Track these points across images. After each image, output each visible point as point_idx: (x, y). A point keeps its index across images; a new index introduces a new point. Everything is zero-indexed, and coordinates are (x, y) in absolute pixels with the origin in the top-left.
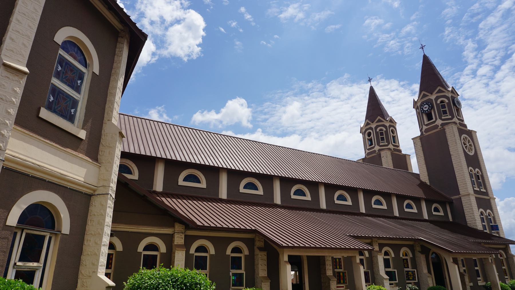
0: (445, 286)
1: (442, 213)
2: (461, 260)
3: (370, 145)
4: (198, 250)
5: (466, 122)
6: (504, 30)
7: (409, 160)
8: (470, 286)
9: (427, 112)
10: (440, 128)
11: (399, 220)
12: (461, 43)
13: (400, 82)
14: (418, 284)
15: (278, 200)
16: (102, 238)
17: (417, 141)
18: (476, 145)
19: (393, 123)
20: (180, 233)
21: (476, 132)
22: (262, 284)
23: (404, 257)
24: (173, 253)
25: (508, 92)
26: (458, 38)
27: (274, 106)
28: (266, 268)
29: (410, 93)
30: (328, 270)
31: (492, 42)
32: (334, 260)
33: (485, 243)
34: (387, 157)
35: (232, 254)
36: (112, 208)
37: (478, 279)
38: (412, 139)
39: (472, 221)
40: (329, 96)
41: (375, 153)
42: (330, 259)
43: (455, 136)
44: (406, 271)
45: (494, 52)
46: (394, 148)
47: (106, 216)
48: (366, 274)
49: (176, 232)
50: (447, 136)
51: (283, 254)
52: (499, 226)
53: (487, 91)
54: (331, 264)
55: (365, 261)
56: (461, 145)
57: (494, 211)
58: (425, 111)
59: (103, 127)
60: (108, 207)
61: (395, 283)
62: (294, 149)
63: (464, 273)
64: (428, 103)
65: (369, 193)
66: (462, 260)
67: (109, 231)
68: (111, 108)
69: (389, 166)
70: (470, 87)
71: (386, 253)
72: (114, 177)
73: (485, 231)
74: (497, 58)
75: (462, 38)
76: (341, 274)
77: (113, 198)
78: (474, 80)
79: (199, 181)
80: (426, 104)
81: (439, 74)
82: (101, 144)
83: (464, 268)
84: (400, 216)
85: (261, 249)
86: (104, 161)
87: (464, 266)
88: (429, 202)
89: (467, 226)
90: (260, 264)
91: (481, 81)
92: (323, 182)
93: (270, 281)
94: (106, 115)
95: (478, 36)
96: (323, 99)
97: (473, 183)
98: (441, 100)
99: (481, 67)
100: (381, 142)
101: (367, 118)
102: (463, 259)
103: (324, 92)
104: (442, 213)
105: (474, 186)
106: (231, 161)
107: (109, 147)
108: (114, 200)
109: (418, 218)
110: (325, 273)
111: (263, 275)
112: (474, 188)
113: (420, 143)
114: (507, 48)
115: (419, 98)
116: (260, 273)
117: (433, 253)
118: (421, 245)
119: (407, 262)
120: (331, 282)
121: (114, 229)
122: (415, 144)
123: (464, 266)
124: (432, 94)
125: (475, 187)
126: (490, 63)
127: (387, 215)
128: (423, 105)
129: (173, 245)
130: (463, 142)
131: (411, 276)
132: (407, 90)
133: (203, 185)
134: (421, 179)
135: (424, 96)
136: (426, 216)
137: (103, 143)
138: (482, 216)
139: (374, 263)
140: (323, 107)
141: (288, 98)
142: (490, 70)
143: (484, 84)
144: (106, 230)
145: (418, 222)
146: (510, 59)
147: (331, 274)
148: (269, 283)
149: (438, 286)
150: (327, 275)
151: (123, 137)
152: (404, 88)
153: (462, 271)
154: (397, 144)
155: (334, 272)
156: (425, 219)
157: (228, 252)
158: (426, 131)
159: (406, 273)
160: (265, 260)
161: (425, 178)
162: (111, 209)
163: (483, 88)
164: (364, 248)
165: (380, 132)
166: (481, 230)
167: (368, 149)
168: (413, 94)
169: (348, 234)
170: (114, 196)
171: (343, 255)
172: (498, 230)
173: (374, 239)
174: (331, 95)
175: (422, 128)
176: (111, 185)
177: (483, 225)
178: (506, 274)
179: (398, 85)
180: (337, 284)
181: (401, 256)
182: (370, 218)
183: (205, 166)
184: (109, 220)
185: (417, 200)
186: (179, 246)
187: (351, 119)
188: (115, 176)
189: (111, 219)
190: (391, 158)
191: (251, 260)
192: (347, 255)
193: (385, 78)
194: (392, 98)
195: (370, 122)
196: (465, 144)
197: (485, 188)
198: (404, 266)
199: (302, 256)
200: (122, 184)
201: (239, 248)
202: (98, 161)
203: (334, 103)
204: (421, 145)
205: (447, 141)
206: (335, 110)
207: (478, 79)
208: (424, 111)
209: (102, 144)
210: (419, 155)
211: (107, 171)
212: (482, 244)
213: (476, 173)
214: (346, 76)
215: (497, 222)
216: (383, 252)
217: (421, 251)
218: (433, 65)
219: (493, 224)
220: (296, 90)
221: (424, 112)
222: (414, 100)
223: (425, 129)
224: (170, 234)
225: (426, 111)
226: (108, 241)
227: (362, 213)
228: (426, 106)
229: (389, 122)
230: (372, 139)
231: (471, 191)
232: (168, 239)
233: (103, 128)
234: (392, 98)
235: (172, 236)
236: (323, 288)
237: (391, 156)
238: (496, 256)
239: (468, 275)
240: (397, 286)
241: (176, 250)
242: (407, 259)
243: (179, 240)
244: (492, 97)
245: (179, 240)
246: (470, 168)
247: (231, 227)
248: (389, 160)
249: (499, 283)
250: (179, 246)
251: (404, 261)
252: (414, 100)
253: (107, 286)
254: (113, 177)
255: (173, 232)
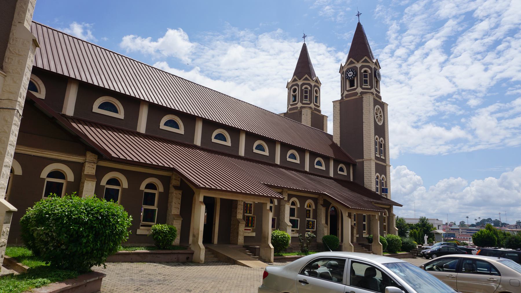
0: (337, 236)
1: (345, 173)
2: (353, 215)
3: (294, 101)
4: (109, 182)
5: (382, 94)
6: (424, 19)
7: (326, 121)
8: (357, 237)
9: (350, 78)
10: (359, 96)
11: (309, 175)
12: (387, 23)
13: (328, 47)
14: (315, 233)
15: (198, 141)
16: (5, 158)
17: (337, 104)
18: (385, 116)
19: (318, 83)
20: (91, 162)
21: (388, 105)
22: (173, 222)
23: (307, 209)
24: (82, 183)
25: (415, 76)
26: (386, 17)
27: (202, 47)
28: (179, 206)
29: (335, 60)
30: (239, 214)
31: (412, 28)
32: (245, 205)
33: (376, 203)
34: (307, 115)
35: (146, 189)
36: (18, 126)
37: (364, 231)
38: (333, 102)
39: (369, 183)
40: (259, 48)
41: (297, 110)
42: (242, 204)
43: (371, 105)
44: (307, 221)
45: (411, 38)
46: (315, 108)
47: (11, 134)
48: (273, 220)
49: (87, 161)
50: (363, 104)
51: (199, 194)
52: (388, 190)
53: (399, 72)
54: (242, 208)
55: (274, 208)
56: (373, 115)
57: (388, 176)
58: (349, 77)
59: (12, 30)
60: (14, 124)
61: (296, 230)
62: (221, 93)
63: (354, 226)
64: (353, 70)
65: (286, 147)
66: (355, 215)
67: (12, 151)
68: (23, 8)
69: (307, 124)
70: (386, 65)
71: (293, 204)
72: (23, 91)
73: (377, 193)
74: (413, 43)
75: (389, 18)
76: (250, 218)
77: (20, 115)
78: (390, 59)
79: (116, 111)
80: (351, 71)
81: (368, 44)
82: (7, 50)
83: (355, 222)
84: (310, 172)
85: (176, 188)
86: (11, 71)
87: (355, 221)
88: (337, 162)
89: (364, 187)
90: (173, 202)
91: (396, 62)
92: (245, 129)
93: (182, 219)
94: (16, 15)
95: (402, 20)
96: (252, 50)
97: (376, 149)
98: (365, 69)
99: (398, 48)
100: (304, 99)
101: (295, 74)
102: (355, 214)
103: (254, 43)
104: (345, 173)
105: (376, 153)
106: (158, 91)
107: (19, 55)
108: (21, 117)
109: (324, 175)
110: (236, 217)
111: (176, 213)
112: (376, 155)
113: (339, 106)
114: (422, 36)
115: (346, 63)
116: (173, 210)
117: (333, 207)
118: (324, 199)
119: (310, 212)
120: (240, 224)
121: (19, 151)
122: (334, 107)
123: (355, 221)
124: (358, 62)
125: (377, 154)
126: (406, 47)
127: (299, 169)
128: (349, 71)
129: (83, 174)
130: (376, 112)
131: (310, 225)
132: (332, 56)
133: (121, 115)
134: (334, 140)
135: (352, 63)
136: (332, 175)
137: (10, 48)
138: (377, 180)
139: (281, 211)
140: (251, 58)
141: (218, 42)
142: (406, 53)
143: (398, 64)
144: (9, 150)
145: (324, 179)
146: (423, 46)
147: (241, 217)
148: (181, 221)
149: (332, 236)
150: (237, 218)
151: (37, 47)
152: (330, 54)
153: (353, 224)
154: (318, 104)
155: (244, 216)
156: (330, 177)
157: (143, 187)
158: (347, 96)
159: (307, 222)
160: (179, 199)
161: (337, 140)
162: (17, 127)
163: (397, 68)
164: (276, 196)
165: (305, 90)
166: (374, 192)
167: (291, 105)
168: (337, 61)
169: (262, 182)
170: (21, 112)
171: (254, 201)
172: (387, 193)
173: (285, 190)
174: (261, 47)
175: (344, 93)
176: (19, 99)
177: (376, 187)
178: (385, 229)
179: (326, 50)
180: (245, 227)
181: (306, 207)
182: (284, 170)
183: (125, 95)
184: (13, 139)
185: (327, 159)
186: (89, 176)
187: (276, 75)
188: (25, 90)
189: (16, 138)
190: (311, 116)
191: (165, 198)
192: (259, 201)
193: (315, 40)
194: (318, 62)
195: (297, 78)
196: (376, 114)
197: (385, 156)
198: (307, 216)
199: (216, 198)
200: (30, 101)
201: (153, 184)
202: (2, 69)
203: (263, 56)
204: (339, 109)
205: (362, 109)
206: (262, 63)
207: (394, 58)
208: (348, 77)
209: (9, 50)
210: (336, 118)
211: (15, 82)
212: (373, 203)
213: (380, 141)
214: (279, 31)
215: (388, 186)
216: (291, 202)
217: (323, 204)
218: (365, 34)
219: (384, 187)
220: (227, 36)
221: (348, 78)
222: (341, 64)
223: (346, 95)
224: (80, 163)
225: (350, 77)
226: (11, 162)
227: (277, 165)
228: (351, 72)
229: (315, 82)
230: (296, 96)
231: (373, 157)
232: (78, 168)
233: (11, 31)
234: (318, 62)
235: (81, 166)
236: (231, 229)
237: (311, 115)
238: (381, 214)
239: (356, 228)
240: (297, 233)
241: (86, 179)
242: (310, 210)
243: (90, 169)
244: (402, 78)
245: (90, 169)
246: (377, 136)
247: (148, 162)
248: (309, 119)
249: (379, 235)
250: (89, 176)
251: (307, 212)
252: (341, 64)
253: (8, 210)
254: (21, 91)
255: (84, 161)
